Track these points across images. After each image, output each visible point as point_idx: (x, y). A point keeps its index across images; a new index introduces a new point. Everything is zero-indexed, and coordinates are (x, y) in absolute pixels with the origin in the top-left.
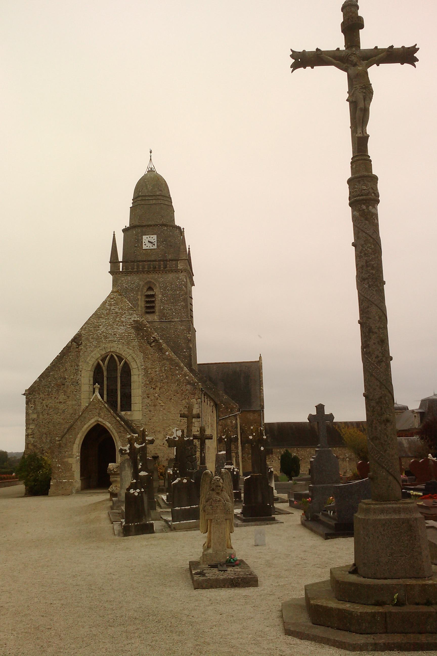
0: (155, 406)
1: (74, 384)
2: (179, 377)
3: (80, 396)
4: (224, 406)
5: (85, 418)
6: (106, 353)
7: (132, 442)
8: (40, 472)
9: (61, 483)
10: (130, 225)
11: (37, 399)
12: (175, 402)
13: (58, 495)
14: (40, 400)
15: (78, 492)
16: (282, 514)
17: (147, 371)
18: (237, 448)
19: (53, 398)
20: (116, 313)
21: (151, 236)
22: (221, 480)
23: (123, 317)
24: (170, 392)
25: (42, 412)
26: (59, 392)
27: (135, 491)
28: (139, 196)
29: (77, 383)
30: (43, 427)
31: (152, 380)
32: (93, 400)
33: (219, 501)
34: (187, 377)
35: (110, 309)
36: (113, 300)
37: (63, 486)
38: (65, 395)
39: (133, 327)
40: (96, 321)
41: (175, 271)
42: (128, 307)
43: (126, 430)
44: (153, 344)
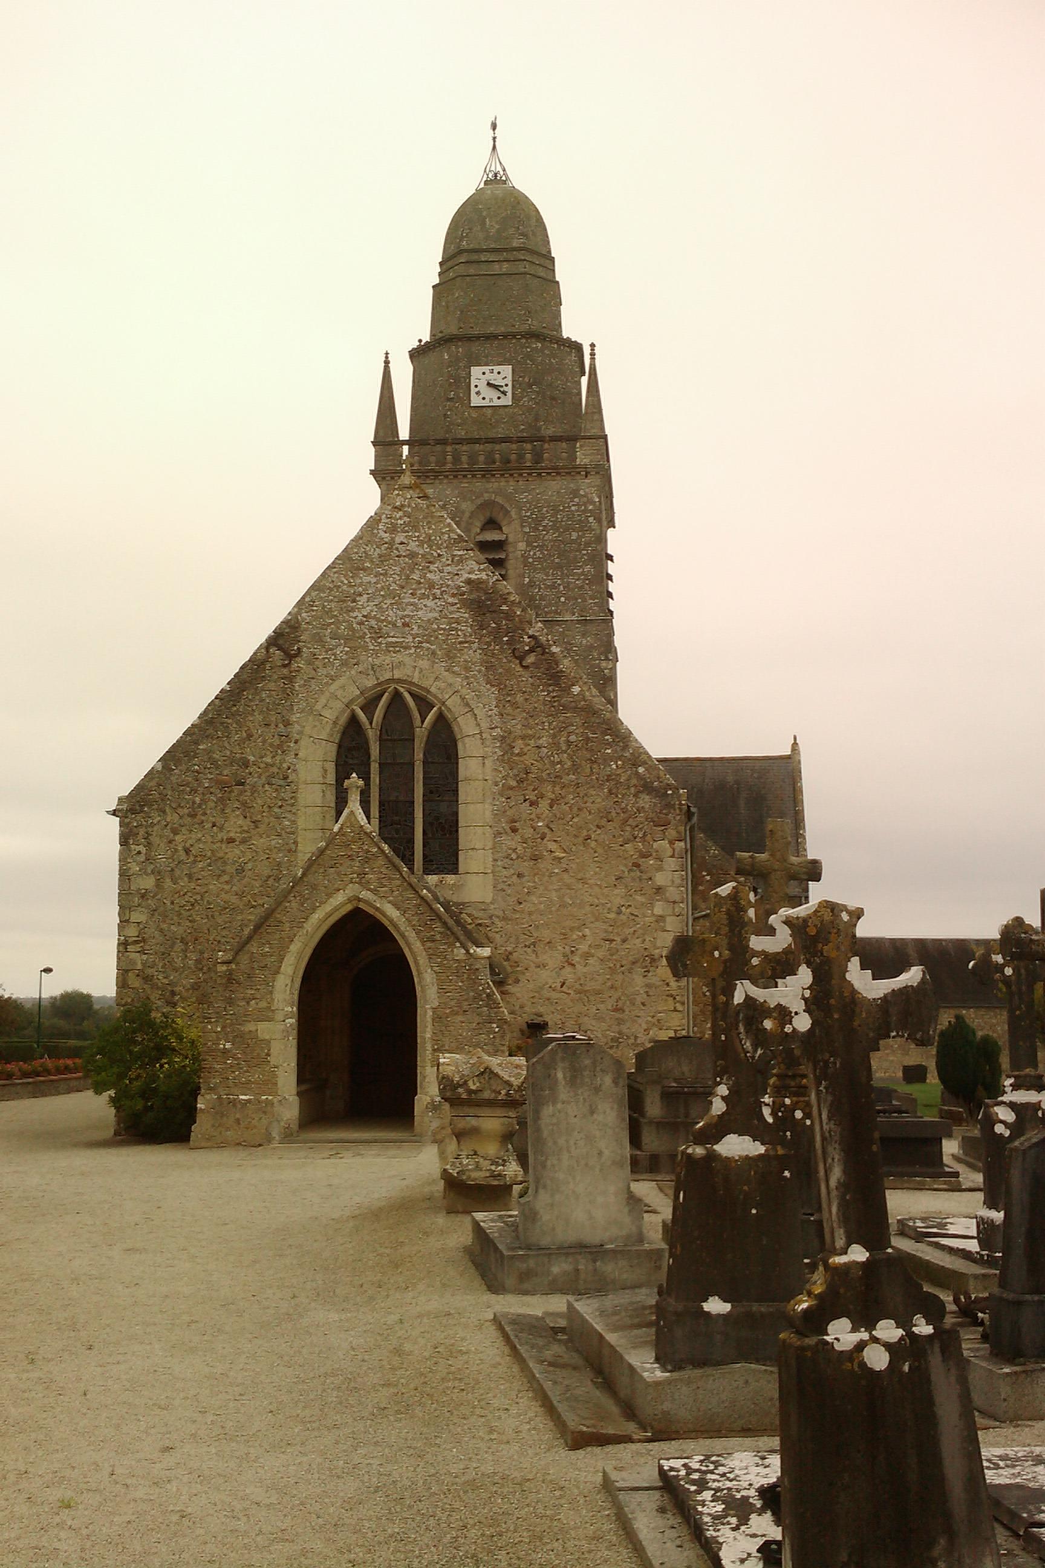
0: (535, 858)
1: (274, 781)
2: (614, 766)
3: (294, 822)
4: (708, 878)
5: (314, 889)
6: (379, 684)
7: (828, 950)
8: (162, 1066)
9: (234, 1103)
10: (432, 335)
11: (155, 828)
12: (600, 850)
13: (222, 1145)
14: (167, 832)
15: (288, 1137)
17: (509, 745)
19: (208, 826)
20: (412, 555)
21: (497, 368)
23: (432, 567)
24: (584, 815)
25: (172, 870)
26: (225, 805)
27: (865, 1336)
28: (461, 252)
29: (284, 779)
30: (175, 918)
31: (527, 773)
32: (341, 829)
34: (641, 770)
35: (391, 543)
36: (401, 513)
37: (238, 1116)
38: (245, 817)
39: (466, 604)
40: (346, 582)
41: (567, 473)
42: (449, 537)
43: (453, 933)
44: (531, 659)
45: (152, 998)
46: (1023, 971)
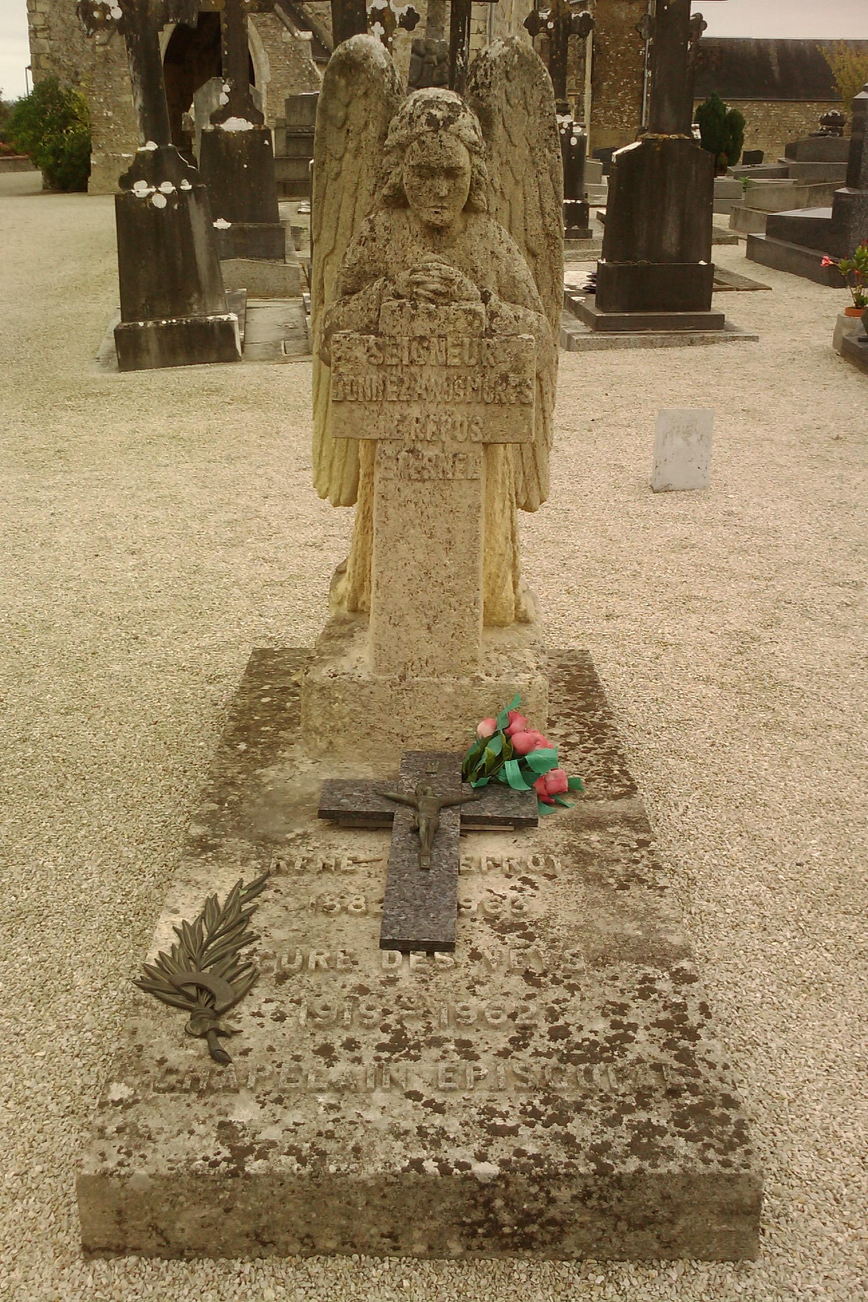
8: (68, 132)
16: (731, 289)
18: (581, 86)
22: (467, 122)
33: (437, 297)
43: (281, 19)
45: (61, 77)
46: (561, 25)
